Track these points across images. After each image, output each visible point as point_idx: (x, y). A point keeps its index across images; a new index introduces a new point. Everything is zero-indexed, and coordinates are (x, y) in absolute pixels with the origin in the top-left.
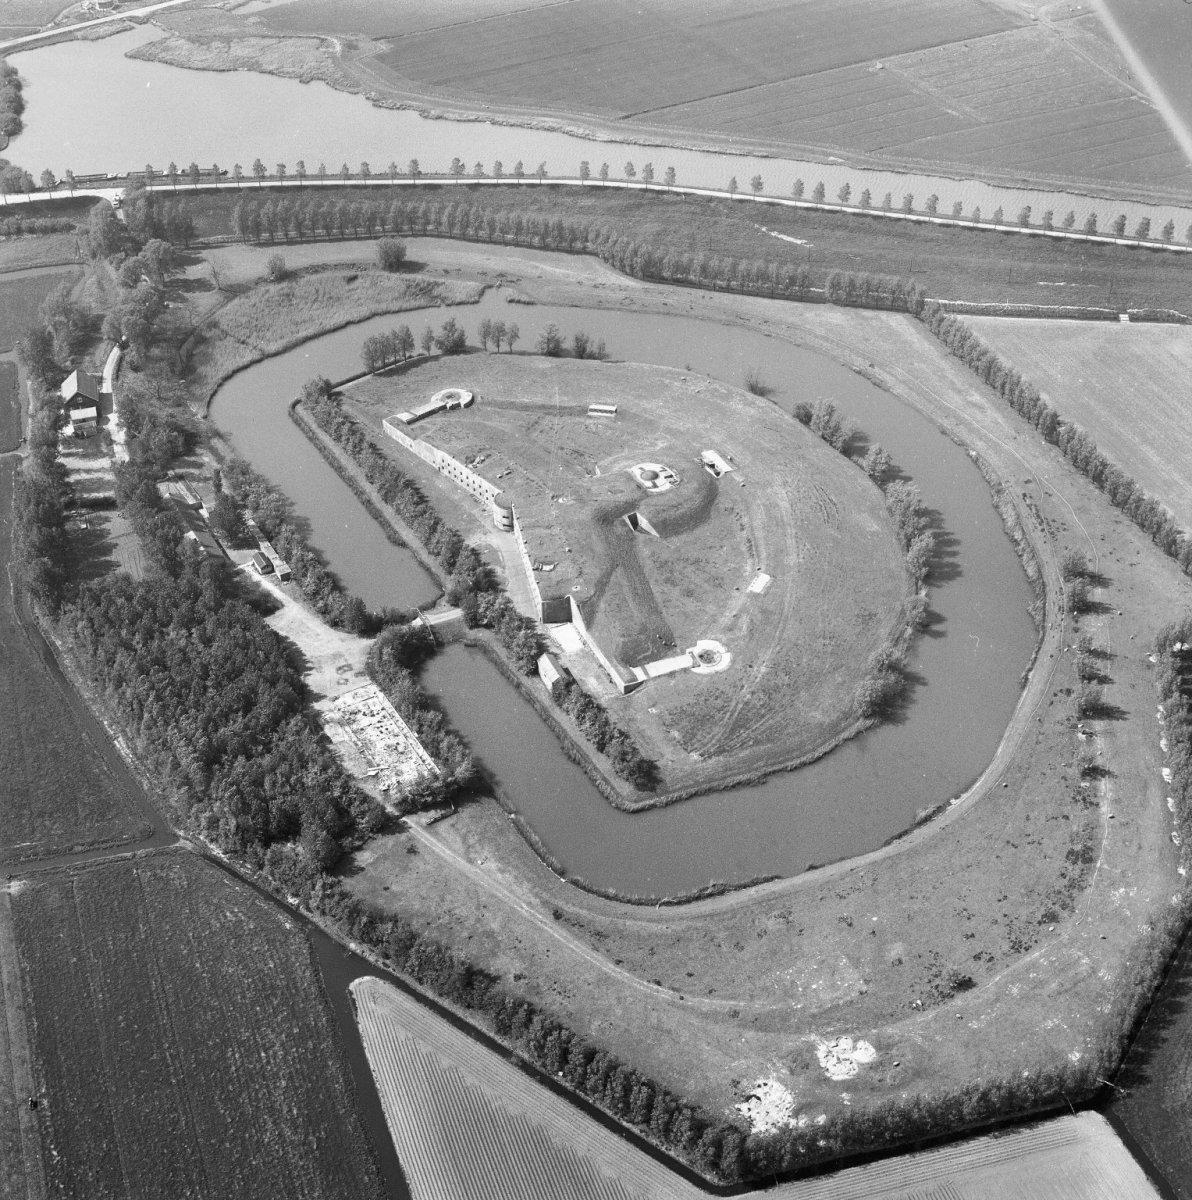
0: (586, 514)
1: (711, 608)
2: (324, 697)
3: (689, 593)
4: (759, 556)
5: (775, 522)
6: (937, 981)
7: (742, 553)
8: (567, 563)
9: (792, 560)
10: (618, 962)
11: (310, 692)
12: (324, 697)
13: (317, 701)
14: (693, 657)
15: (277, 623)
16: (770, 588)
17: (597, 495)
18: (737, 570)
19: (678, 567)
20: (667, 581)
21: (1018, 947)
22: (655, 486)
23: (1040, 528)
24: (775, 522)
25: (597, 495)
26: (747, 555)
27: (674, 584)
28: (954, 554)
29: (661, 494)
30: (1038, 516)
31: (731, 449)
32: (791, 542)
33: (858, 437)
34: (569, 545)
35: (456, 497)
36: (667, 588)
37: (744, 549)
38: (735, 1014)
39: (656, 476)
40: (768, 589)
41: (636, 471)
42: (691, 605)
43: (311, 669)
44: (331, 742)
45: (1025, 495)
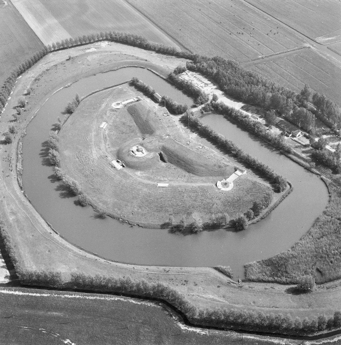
0: (158, 132)
1: (118, 120)
2: (214, 89)
3: (124, 124)
4: (103, 135)
5: (97, 145)
6: (73, 60)
7: (109, 137)
8: (159, 116)
9: (93, 133)
10: (133, 56)
11: (219, 90)
12: (214, 89)
13: (216, 88)
14: (122, 104)
15: (241, 104)
16: (101, 124)
17: (156, 140)
18: (125, 288)
19: (128, 131)
20: (131, 127)
21: (56, 65)
22: (137, 147)
23: (11, 159)
24: (97, 145)
25: (156, 140)
26: (107, 136)
27: (129, 126)
28: (42, 150)
29: (135, 145)
30: (10, 162)
31: (112, 172)
32: (93, 140)
33: (64, 196)
34: (161, 121)
35: (267, 322)
36: (131, 124)
37: (108, 138)
38: (111, 52)
39: (138, 150)
40: (101, 123)
41: (145, 153)
42: (123, 120)
43: (222, 95)
44: (208, 80)
45: (11, 171)
